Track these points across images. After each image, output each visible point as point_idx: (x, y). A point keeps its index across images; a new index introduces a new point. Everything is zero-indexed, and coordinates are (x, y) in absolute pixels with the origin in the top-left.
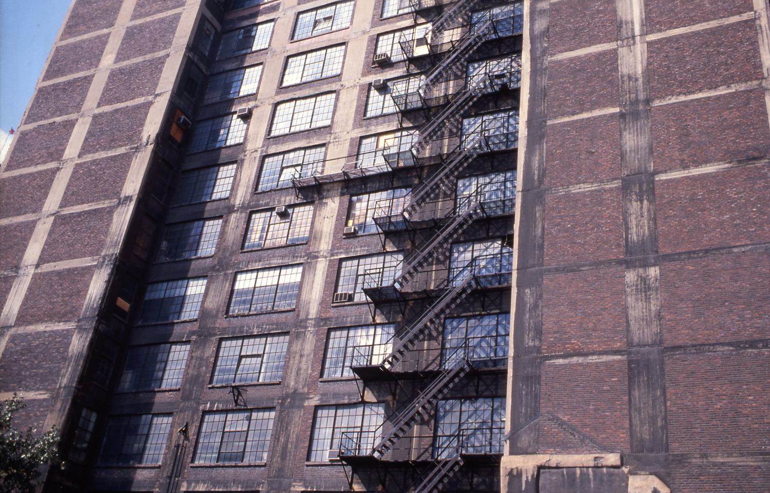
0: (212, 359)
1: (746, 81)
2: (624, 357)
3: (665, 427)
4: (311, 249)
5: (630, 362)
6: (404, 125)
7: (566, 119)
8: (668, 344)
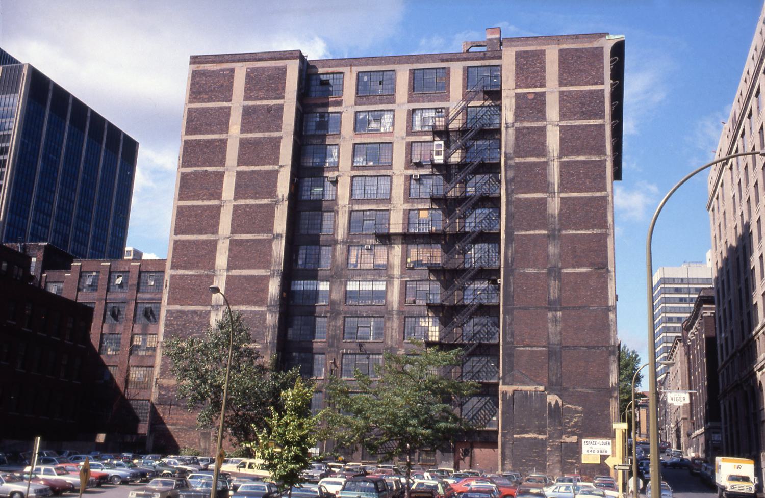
0: (342, 327)
1: (601, 229)
2: (547, 349)
3: (561, 377)
4: (389, 273)
5: (549, 351)
6: (433, 207)
7: (523, 233)
8: (564, 345)
